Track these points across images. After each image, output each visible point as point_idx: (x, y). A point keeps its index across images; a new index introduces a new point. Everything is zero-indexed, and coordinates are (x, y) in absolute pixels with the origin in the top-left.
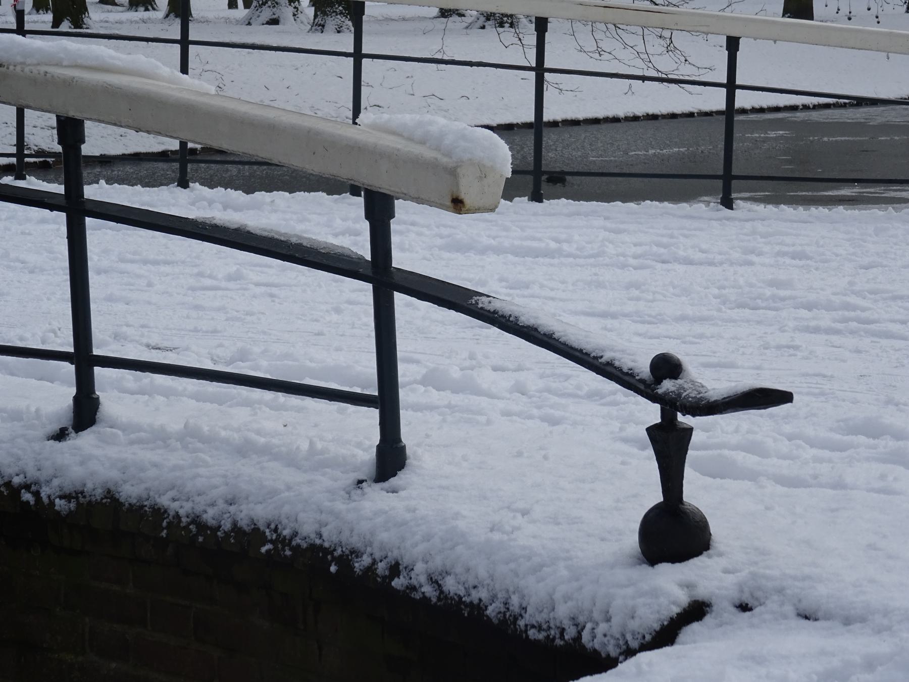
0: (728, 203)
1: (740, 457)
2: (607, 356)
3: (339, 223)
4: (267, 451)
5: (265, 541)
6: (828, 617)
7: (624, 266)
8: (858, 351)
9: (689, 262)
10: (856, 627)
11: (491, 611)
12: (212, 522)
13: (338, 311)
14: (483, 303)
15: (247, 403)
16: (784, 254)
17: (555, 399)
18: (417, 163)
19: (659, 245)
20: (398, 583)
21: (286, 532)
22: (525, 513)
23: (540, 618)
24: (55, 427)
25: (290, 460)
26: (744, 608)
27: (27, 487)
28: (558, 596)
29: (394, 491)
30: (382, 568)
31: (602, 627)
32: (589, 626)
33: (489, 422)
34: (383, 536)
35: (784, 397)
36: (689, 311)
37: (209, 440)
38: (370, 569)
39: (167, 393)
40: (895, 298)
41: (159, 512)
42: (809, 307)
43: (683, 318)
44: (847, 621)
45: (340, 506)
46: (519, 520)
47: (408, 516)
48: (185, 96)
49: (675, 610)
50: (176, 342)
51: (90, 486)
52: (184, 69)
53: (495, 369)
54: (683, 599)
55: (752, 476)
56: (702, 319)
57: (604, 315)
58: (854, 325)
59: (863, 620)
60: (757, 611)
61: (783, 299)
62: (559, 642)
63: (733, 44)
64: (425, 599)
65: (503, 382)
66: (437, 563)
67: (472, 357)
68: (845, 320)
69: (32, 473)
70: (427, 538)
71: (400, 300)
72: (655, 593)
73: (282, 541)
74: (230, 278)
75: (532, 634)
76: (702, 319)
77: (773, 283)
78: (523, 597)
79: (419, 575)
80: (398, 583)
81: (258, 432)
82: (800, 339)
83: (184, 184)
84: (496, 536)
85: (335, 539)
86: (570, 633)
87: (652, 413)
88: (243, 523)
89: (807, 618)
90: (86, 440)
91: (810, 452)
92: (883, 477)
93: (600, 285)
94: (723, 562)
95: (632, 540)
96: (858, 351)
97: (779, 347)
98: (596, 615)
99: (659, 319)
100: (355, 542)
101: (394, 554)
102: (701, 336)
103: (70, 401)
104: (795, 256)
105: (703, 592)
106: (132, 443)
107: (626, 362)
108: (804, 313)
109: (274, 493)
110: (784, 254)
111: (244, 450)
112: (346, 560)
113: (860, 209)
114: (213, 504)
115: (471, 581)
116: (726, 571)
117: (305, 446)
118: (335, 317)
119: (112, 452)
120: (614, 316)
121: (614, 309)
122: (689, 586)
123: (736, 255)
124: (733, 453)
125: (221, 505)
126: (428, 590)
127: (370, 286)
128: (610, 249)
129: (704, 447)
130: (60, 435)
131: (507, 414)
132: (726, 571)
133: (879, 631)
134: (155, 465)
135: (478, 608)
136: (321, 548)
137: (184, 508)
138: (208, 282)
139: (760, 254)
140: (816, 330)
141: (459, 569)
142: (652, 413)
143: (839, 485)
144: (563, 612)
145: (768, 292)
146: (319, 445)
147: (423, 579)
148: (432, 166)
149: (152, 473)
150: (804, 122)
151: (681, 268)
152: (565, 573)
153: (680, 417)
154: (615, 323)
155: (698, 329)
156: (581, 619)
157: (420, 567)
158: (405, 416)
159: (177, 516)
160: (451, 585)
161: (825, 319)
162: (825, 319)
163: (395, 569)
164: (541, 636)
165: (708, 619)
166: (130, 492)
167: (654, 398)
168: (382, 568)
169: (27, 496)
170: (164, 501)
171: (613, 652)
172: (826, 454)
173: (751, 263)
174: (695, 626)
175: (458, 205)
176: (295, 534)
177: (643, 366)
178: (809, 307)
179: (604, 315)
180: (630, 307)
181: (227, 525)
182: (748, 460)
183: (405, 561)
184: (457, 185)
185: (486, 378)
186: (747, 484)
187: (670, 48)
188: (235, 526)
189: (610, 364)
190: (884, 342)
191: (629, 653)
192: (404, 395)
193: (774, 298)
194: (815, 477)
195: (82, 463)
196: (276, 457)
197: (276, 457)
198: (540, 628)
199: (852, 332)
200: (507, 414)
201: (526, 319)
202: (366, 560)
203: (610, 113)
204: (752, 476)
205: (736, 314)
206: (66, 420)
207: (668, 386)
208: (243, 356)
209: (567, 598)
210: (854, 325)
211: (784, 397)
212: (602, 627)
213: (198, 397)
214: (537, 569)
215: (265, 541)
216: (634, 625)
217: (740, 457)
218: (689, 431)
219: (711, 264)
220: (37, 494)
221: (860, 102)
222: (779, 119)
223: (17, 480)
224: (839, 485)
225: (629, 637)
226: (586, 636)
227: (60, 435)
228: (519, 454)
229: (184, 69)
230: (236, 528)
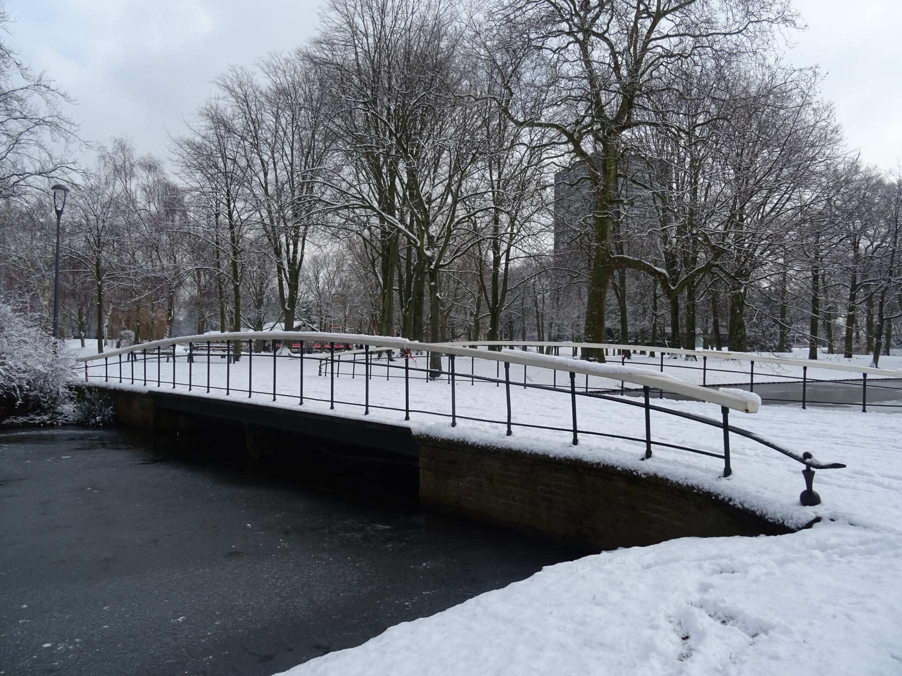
0: (804, 408)
1: (824, 478)
2: (790, 451)
3: (701, 409)
4: (694, 467)
5: (695, 489)
6: (859, 525)
7: (778, 423)
8: (851, 450)
9: (796, 423)
10: (868, 529)
11: (757, 513)
12: (681, 483)
13: (705, 431)
14: (754, 435)
15: (689, 455)
16: (823, 422)
17: (768, 458)
18: (736, 401)
19: (787, 418)
20: (731, 503)
21: (701, 488)
22: (766, 489)
23: (772, 517)
24: (642, 457)
25: (701, 470)
26: (832, 520)
27: (635, 471)
28: (777, 511)
29: (729, 480)
30: (726, 499)
31: (790, 521)
32: (786, 520)
33: (752, 464)
34: (727, 491)
35: (844, 466)
36: (800, 437)
37: (680, 463)
38: (724, 499)
39: (668, 451)
40: (859, 436)
41: (667, 480)
42: (835, 437)
43: (798, 438)
44: (865, 527)
45: (715, 482)
46: (764, 491)
47: (733, 487)
48: (675, 382)
49: (812, 519)
50: (666, 437)
51: (650, 473)
52: (662, 371)
53: (750, 449)
54: (813, 516)
55: (830, 484)
56: (803, 439)
57: (776, 436)
58: (848, 443)
59: (870, 527)
60: (836, 521)
61: (826, 435)
62: (777, 523)
63: (805, 368)
64: (739, 508)
65: (752, 453)
66: (742, 499)
67: (742, 446)
68: (845, 442)
69: (636, 468)
70: (739, 493)
71: (730, 433)
72: (806, 514)
73: (699, 490)
74: (676, 422)
75: (770, 520)
76: (803, 439)
77: (822, 430)
78: (767, 510)
79: (737, 502)
80: (731, 503)
81: (692, 462)
82: (833, 446)
83: (661, 398)
84: (759, 494)
85: (714, 490)
86: (781, 521)
87: (804, 467)
88: (689, 485)
89: (852, 525)
90: (649, 461)
91: (844, 478)
92: (869, 487)
93: (773, 428)
94: (824, 507)
95: (798, 499)
96: (851, 450)
97: (828, 448)
98: (789, 518)
99: (791, 438)
100: (719, 492)
101: (730, 496)
102: (804, 444)
103: (645, 452)
104: (826, 423)
105: (819, 515)
106: (660, 462)
107: (795, 453)
108: (833, 439)
109: (697, 478)
110: (823, 422)
111: (688, 466)
112: (717, 496)
113: (827, 410)
114: (681, 479)
115: (752, 505)
116: (826, 510)
117: (704, 466)
118: (704, 433)
119: (656, 464)
120: (779, 437)
121: (779, 435)
122: (815, 513)
123: (809, 422)
124: (822, 477)
125: (684, 479)
126: (740, 506)
127: (722, 429)
128: (774, 419)
129: (817, 475)
130: (643, 459)
131: (755, 461)
132: (826, 510)
133: (876, 531)
134: (666, 468)
135: (754, 512)
136: (710, 492)
137: (674, 480)
138: (671, 423)
139: (816, 422)
140: (837, 444)
141: (748, 502)
142: (804, 467)
143: (855, 488)
144: (779, 516)
145: (822, 433)
146: (708, 467)
147: (738, 503)
148: (740, 402)
149: (666, 470)
150: (816, 386)
151: (794, 425)
152: (779, 506)
153: (812, 468)
154: (779, 439)
155: (803, 441)
156: (784, 518)
157: (737, 500)
158: (731, 461)
159: (672, 481)
160: (746, 505)
161: (840, 441)
162: (840, 441)
163: (730, 500)
164: (772, 521)
165: (821, 522)
166: (660, 474)
167: (804, 463)
168: (726, 499)
169: (635, 473)
170: (669, 477)
171: (794, 528)
172: (849, 479)
173: (813, 424)
174: (818, 523)
175: (747, 411)
176: (703, 488)
177: (801, 455)
178: (835, 437)
179: (776, 436)
180: (783, 435)
181: (685, 485)
182: (827, 479)
183: (733, 498)
184: (747, 406)
185: (748, 452)
186: (827, 486)
187: (779, 366)
188: (687, 485)
189: (791, 453)
190: (859, 448)
191: (799, 529)
192: (731, 455)
193: (823, 434)
194: (848, 486)
195: (648, 467)
196: (697, 469)
197: (697, 469)
198: (772, 519)
199: (848, 445)
200: (755, 461)
201: (766, 440)
202: (722, 497)
203: (763, 382)
204: (830, 484)
205: (812, 438)
206: (644, 456)
207: (808, 460)
208: (683, 442)
209: (779, 512)
210: (848, 443)
211: (844, 466)
212: (790, 521)
213: (674, 452)
214: (771, 503)
215: (695, 489)
216: (800, 521)
217: (824, 478)
218: (814, 473)
219: (802, 424)
220: (637, 473)
221: (817, 381)
222: (888, 400)
223: (632, 469)
224: (855, 488)
225: (798, 524)
226: (785, 523)
227: (643, 459)
228: (762, 473)
229: (662, 371)
230: (687, 485)
